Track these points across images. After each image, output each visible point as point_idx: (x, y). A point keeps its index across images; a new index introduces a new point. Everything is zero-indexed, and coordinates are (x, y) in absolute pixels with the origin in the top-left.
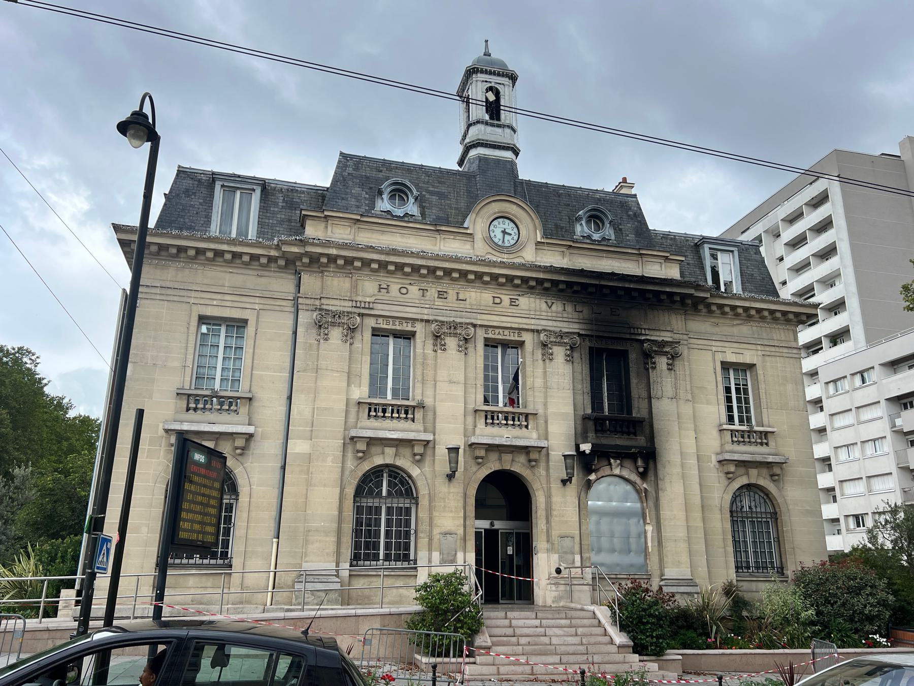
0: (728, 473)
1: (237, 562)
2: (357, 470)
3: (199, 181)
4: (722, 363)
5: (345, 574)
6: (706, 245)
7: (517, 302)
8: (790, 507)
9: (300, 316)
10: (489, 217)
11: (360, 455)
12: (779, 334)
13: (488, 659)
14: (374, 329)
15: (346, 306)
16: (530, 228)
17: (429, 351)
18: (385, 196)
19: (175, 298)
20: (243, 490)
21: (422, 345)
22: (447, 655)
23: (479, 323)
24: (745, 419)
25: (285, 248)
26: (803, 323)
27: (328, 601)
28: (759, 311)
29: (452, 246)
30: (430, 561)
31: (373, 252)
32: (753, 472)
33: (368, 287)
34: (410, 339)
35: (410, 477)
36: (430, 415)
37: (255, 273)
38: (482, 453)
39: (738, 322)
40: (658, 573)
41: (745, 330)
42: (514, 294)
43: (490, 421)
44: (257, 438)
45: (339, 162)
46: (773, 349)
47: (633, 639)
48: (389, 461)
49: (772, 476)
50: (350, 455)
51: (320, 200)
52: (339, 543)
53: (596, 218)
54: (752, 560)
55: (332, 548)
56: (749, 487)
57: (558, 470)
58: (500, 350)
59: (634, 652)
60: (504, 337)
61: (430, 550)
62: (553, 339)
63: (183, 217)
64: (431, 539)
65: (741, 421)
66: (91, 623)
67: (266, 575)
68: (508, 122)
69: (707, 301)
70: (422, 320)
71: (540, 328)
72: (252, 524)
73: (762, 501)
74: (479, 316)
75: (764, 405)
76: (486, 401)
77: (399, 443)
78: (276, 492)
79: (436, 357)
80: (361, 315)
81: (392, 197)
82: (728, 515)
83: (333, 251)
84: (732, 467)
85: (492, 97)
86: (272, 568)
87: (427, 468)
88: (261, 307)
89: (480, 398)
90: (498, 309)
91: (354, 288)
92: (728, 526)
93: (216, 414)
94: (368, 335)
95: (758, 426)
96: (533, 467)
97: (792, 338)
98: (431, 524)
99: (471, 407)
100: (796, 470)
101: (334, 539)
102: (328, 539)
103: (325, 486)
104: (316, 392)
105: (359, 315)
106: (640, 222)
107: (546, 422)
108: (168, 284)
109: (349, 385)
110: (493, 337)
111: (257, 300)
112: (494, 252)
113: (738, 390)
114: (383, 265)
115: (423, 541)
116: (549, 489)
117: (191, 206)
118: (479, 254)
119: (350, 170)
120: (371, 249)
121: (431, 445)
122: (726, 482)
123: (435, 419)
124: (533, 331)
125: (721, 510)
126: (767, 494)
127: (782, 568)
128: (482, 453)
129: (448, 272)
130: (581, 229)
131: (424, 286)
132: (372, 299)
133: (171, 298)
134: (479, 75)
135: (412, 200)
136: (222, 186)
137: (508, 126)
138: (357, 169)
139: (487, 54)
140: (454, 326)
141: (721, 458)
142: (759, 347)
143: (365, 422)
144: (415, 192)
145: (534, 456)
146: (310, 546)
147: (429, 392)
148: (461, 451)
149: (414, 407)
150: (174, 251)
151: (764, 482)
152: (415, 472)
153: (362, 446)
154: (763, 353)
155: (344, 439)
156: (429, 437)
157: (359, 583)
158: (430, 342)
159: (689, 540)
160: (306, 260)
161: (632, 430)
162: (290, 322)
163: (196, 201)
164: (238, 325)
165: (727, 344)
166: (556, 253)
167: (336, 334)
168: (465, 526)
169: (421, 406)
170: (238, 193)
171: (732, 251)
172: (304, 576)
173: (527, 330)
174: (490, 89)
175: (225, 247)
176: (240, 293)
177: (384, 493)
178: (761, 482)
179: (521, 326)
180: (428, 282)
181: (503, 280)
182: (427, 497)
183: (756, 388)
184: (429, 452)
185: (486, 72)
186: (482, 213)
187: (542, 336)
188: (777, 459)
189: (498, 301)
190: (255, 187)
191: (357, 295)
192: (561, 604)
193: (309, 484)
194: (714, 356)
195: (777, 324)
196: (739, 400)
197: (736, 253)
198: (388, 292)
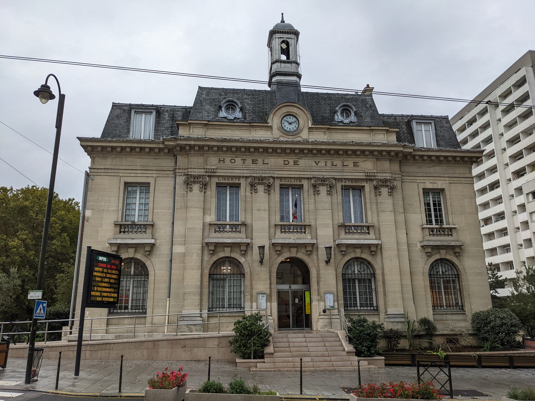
0: (427, 253)
1: (149, 311)
2: (209, 260)
3: (124, 110)
4: (423, 189)
5: (205, 316)
6: (414, 121)
7: (298, 163)
8: (467, 271)
9: (177, 179)
10: (281, 115)
11: (211, 252)
12: (460, 171)
13: (271, 360)
14: (217, 183)
15: (202, 172)
16: (305, 119)
17: (248, 194)
18: (223, 109)
19: (112, 174)
20: (151, 273)
21: (244, 191)
22: (249, 358)
23: (276, 176)
24: (439, 221)
25: (166, 143)
26: (475, 162)
27: (196, 330)
28: (446, 157)
29: (259, 134)
30: (251, 308)
31: (214, 141)
32: (443, 252)
33: (213, 161)
35: (240, 263)
36: (250, 228)
38: (279, 248)
39: (435, 164)
40: (384, 311)
41: (438, 169)
42: (295, 158)
44: (157, 245)
45: (198, 92)
46: (456, 179)
47: (355, 348)
48: (131, 256)
49: (455, 253)
50: (206, 252)
51: (186, 114)
52: (201, 300)
53: (346, 111)
54: (445, 305)
55: (197, 302)
56: (441, 260)
57: (322, 254)
59: (356, 355)
61: (252, 302)
62: (319, 182)
63: (115, 130)
64: (252, 296)
65: (437, 221)
66: (83, 342)
67: (164, 317)
68: (294, 59)
69: (412, 153)
70: (243, 177)
71: (311, 176)
72: (156, 291)
73: (450, 268)
74: (276, 172)
75: (450, 212)
77: (233, 246)
78: (168, 273)
80: (210, 177)
81: (227, 108)
82: (427, 277)
83: (192, 143)
84: (429, 250)
85: (284, 46)
86: (167, 314)
87: (249, 258)
89: (278, 218)
90: (287, 167)
91: (206, 161)
93: (135, 234)
94: (214, 187)
95: (447, 225)
96: (309, 255)
97: (468, 171)
98: (252, 288)
99: (273, 223)
100: (470, 250)
101: (199, 297)
102: (195, 297)
103: (193, 269)
104: (186, 219)
105: (208, 176)
106: (373, 110)
107: (316, 229)
109: (204, 214)
110: (285, 183)
111: (155, 172)
112: (284, 136)
113: (435, 205)
114: (220, 148)
115: (248, 297)
116: (318, 266)
117: (120, 124)
118: (275, 137)
119: (204, 96)
120: (211, 139)
121: (315, 246)
122: (426, 258)
123: (252, 230)
124: (308, 178)
126: (453, 264)
127: (462, 306)
128: (429, 250)
129: (257, 149)
130: (338, 117)
131: (244, 157)
132: (215, 167)
133: (110, 174)
134: (277, 34)
135: (238, 110)
137: (294, 62)
138: (208, 94)
139: (283, 21)
140: (324, 180)
141: (422, 244)
142: (447, 179)
144: (240, 105)
145: (373, 249)
146: (186, 302)
147: (249, 216)
148: (333, 248)
150: (110, 149)
151: (450, 257)
152: (242, 260)
153: (212, 248)
154: (450, 182)
155: (202, 244)
156: (249, 241)
157: (214, 321)
158: (248, 188)
159: (402, 292)
160: (178, 148)
161: (450, 233)
162: (173, 183)
164: (145, 186)
167: (196, 188)
168: (270, 288)
169: (244, 224)
171: (431, 123)
172: (182, 317)
173: (304, 178)
174: (283, 42)
175: (135, 145)
177: (132, 273)
178: (448, 257)
179: (300, 176)
180: (246, 155)
181: (315, 152)
183: (446, 203)
184: (249, 249)
185: (280, 32)
186: (277, 113)
187: (313, 181)
188: (457, 244)
189: (286, 163)
190: (430, 121)
191: (207, 165)
192: (326, 330)
193: (184, 268)
194: (418, 185)
195: (458, 164)
196: (435, 210)
197: (433, 124)
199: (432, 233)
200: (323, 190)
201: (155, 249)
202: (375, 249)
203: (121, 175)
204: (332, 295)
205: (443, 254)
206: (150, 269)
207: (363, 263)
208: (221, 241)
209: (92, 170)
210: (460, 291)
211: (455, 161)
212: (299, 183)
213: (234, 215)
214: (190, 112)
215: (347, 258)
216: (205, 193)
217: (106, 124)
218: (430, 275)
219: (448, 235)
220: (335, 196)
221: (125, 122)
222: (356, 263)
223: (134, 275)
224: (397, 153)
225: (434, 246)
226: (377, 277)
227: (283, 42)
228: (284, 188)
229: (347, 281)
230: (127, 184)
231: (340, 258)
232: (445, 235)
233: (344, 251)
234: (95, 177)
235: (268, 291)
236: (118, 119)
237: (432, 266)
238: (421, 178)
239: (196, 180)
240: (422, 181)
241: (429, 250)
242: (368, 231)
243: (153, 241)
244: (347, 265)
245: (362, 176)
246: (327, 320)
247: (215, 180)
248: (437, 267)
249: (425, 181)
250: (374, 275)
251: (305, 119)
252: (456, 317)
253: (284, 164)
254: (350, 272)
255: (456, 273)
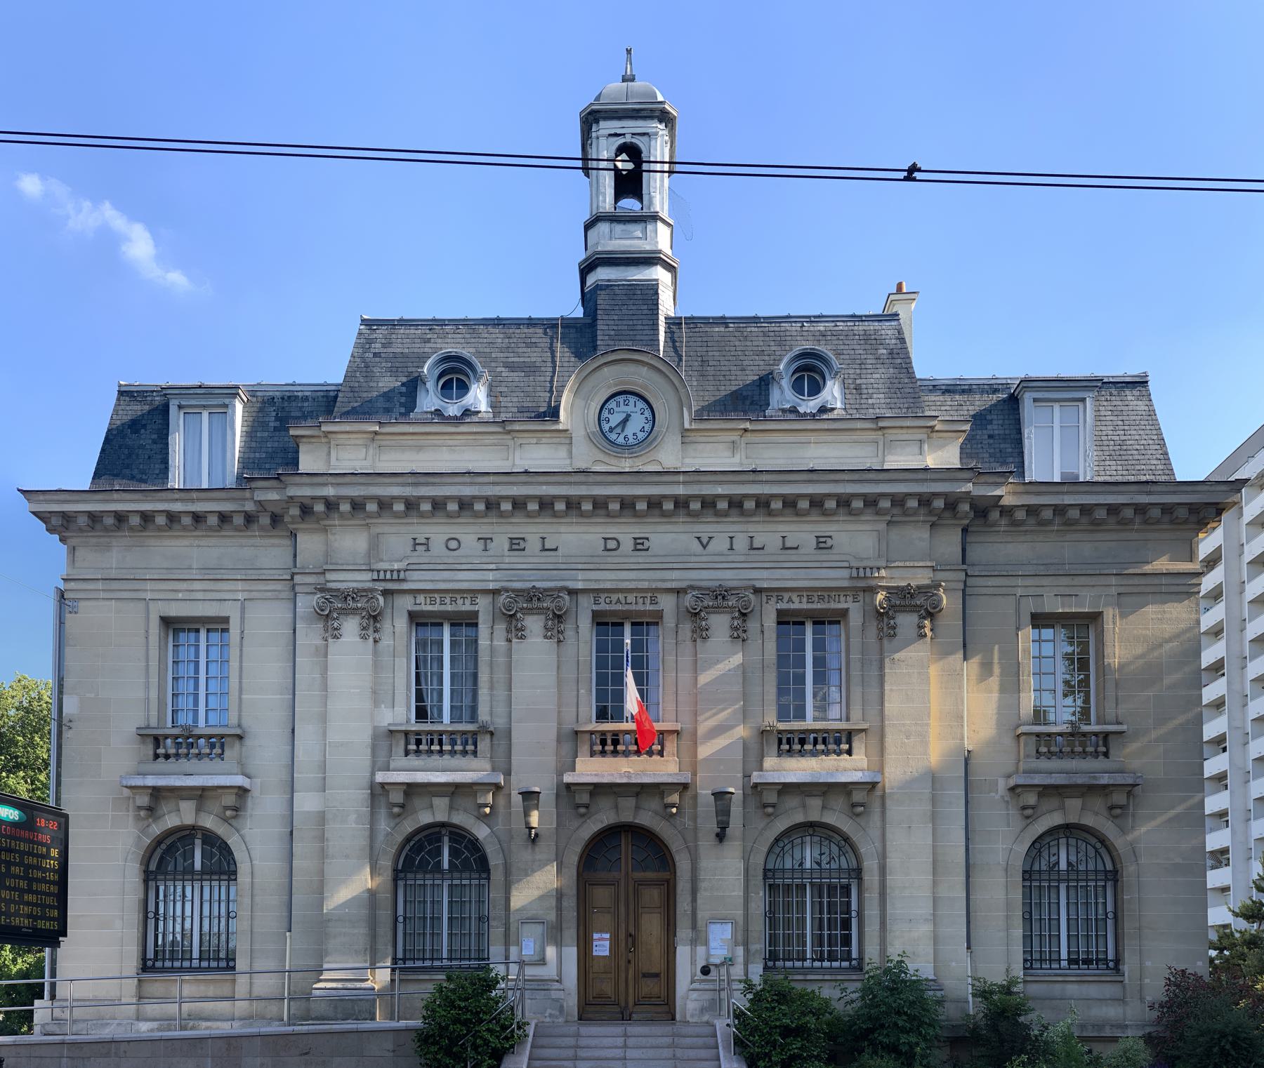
0: (1024, 808)
2: (392, 833)
7: (647, 544)
9: (299, 604)
15: (362, 579)
19: (1148, 589)
23: (580, 586)
32: (1074, 804)
33: (397, 541)
34: (838, 622)
37: (1114, 536)
38: (585, 798)
43: (413, 747)
44: (256, 792)
48: (441, 817)
50: (383, 813)
54: (1064, 955)
56: (1068, 829)
58: (809, 628)
60: (626, 607)
61: (507, 944)
62: (705, 604)
64: (507, 930)
73: (1092, 853)
74: (580, 575)
76: (602, 715)
77: (455, 790)
79: (510, 650)
81: (797, 387)
85: (624, 165)
88: (246, 595)
90: (612, 559)
91: (374, 546)
92: (1018, 895)
93: (195, 761)
95: (1098, 723)
96: (858, 815)
103: (347, 857)
108: (113, 574)
110: (608, 607)
111: (240, 585)
112: (606, 459)
117: (142, 447)
119: (377, 347)
125: (1006, 870)
127: (1117, 961)
128: (1031, 799)
131: (485, 530)
134: (602, 124)
136: (180, 407)
141: (1012, 782)
143: (399, 760)
145: (858, 796)
149: (475, 733)
152: (481, 832)
154: (1122, 590)
158: (501, 627)
159: (935, 919)
160: (295, 511)
163: (146, 438)
165: (1045, 581)
166: (721, 446)
167: (351, 626)
170: (205, 415)
175: (1068, 500)
176: (213, 576)
177: (446, 866)
182: (501, 868)
187: (688, 600)
188: (1119, 779)
189: (612, 544)
198: (428, 550)
199: (1043, 749)
200: (720, 624)
201: (249, 803)
202: (861, 797)
203: (149, 596)
204: (728, 928)
205: (1073, 811)
206: (239, 854)
207: (829, 839)
208: (421, 777)
209: (72, 585)
210: (1116, 917)
211: (1145, 522)
212: (649, 607)
213: (467, 707)
214: (336, 397)
215: (781, 825)
216: (375, 641)
217: (103, 450)
218: (1028, 875)
219: (1096, 754)
220: (754, 643)
221: (154, 442)
222: (1063, 841)
223: (203, 872)
224: (952, 503)
225: (1045, 787)
226: (866, 877)
227: (622, 149)
228: (606, 624)
229: (778, 886)
230: (167, 622)
231: (762, 825)
232: (1084, 754)
233: (773, 806)
234: (82, 604)
235: (552, 916)
236: (137, 432)
237: (1038, 846)
238: (1029, 582)
239: (535, 604)
240: (1031, 591)
241: (1031, 799)
242: (1104, 749)
243: (239, 780)
244: (1037, 846)
245: (839, 578)
246: (708, 996)
247: (405, 604)
248: (1054, 850)
249: (1039, 591)
250: (858, 873)
251: (674, 405)
252: (1093, 990)
253: (606, 550)
254: (788, 865)
255: (1109, 867)
